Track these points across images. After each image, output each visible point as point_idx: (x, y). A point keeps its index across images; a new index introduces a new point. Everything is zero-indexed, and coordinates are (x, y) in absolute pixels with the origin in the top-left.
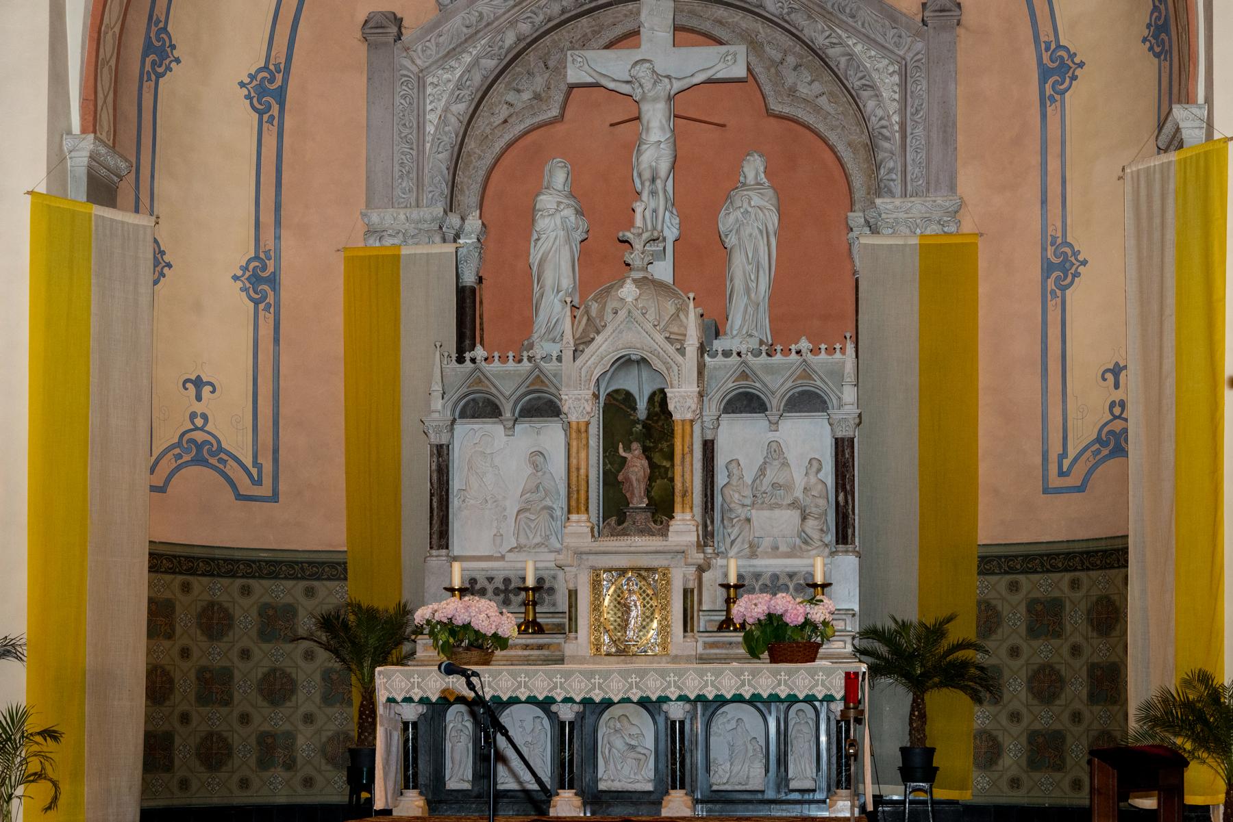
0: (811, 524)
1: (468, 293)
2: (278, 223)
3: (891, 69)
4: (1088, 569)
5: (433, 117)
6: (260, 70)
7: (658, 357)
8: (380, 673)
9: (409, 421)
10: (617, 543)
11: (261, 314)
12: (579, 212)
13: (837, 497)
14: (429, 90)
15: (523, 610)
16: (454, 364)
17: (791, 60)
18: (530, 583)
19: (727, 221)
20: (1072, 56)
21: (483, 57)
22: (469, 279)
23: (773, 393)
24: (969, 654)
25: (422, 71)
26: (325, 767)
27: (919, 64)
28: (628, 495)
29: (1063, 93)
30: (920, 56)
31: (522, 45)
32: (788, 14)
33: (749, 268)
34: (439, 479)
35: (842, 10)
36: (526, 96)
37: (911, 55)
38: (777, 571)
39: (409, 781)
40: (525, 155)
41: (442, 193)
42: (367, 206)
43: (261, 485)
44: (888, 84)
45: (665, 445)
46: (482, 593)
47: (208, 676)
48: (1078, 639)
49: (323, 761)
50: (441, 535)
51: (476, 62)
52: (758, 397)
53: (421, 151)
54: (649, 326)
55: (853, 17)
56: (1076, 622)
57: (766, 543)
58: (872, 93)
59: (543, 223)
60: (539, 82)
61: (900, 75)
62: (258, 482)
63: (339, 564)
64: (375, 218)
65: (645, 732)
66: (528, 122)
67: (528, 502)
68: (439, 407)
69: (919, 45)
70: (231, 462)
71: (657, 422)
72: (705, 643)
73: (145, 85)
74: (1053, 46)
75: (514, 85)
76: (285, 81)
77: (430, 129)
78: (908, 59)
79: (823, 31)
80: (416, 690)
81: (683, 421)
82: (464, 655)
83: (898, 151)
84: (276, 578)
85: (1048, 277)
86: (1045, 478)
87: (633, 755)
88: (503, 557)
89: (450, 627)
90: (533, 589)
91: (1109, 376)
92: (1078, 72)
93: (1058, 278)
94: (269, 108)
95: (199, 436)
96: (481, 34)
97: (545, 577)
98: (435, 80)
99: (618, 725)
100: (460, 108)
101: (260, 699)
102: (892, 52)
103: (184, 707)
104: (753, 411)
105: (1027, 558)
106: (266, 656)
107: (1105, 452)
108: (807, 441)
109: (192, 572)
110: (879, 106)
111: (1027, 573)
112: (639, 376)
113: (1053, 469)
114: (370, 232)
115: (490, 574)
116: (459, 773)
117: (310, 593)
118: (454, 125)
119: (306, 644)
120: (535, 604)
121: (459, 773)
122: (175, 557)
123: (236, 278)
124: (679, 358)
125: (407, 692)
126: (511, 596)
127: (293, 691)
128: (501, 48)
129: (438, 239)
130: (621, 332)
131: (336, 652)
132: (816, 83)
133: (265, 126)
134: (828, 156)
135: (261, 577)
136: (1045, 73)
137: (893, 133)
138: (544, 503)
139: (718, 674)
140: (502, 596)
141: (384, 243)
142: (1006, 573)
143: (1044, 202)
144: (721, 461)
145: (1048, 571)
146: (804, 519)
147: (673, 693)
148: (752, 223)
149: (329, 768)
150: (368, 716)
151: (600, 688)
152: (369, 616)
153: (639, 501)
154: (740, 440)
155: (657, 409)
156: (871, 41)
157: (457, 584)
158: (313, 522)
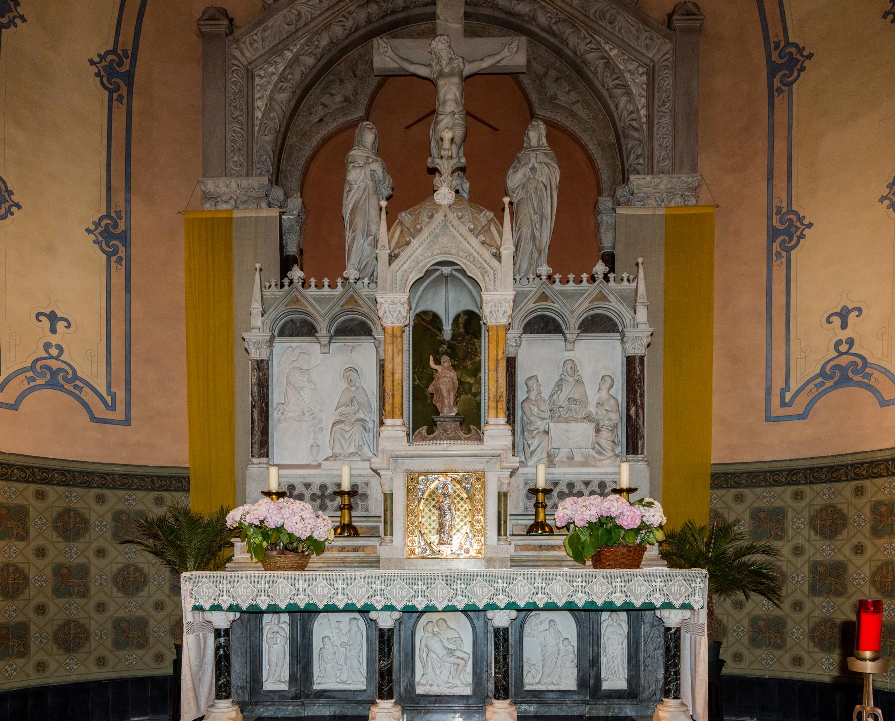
2: (128, 189)
3: (641, 70)
4: (812, 483)
6: (108, 53)
8: (186, 578)
10: (434, 447)
11: (114, 265)
13: (628, 410)
15: (339, 514)
17: (553, 73)
18: (346, 487)
20: (800, 50)
21: (303, 55)
23: (572, 312)
24: (758, 558)
25: (250, 63)
28: (438, 405)
29: (790, 84)
30: (668, 56)
31: (334, 51)
32: (556, 23)
35: (602, 18)
36: (338, 99)
38: (573, 478)
40: (340, 143)
41: (268, 171)
42: (204, 176)
44: (637, 83)
45: (469, 363)
46: (301, 497)
50: (262, 445)
51: (296, 59)
52: (554, 320)
55: (611, 22)
56: (798, 527)
57: (563, 454)
58: (624, 91)
60: (349, 87)
61: (648, 74)
62: (113, 408)
63: (184, 478)
65: (461, 632)
66: (340, 121)
67: (342, 414)
68: (259, 324)
69: (668, 46)
70: (86, 389)
71: (462, 341)
72: (516, 546)
74: (782, 44)
75: (328, 90)
76: (133, 65)
77: (258, 114)
78: (656, 60)
79: (585, 38)
80: (225, 597)
81: (497, 327)
82: (277, 560)
84: (128, 489)
85: (773, 241)
87: (453, 660)
89: (261, 527)
90: (348, 493)
91: (837, 321)
92: (807, 63)
93: (783, 241)
94: (118, 88)
95: (54, 364)
96: (300, 33)
97: (359, 483)
98: (262, 73)
99: (436, 629)
100: (284, 97)
101: (115, 590)
102: (643, 54)
103: (40, 599)
104: (550, 332)
108: (600, 361)
110: (630, 102)
111: (872, 477)
112: (447, 298)
113: (776, 400)
114: (207, 197)
116: (276, 676)
120: (350, 508)
121: (276, 676)
124: (495, 263)
126: (327, 501)
130: (436, 236)
132: (573, 93)
133: (115, 103)
135: (114, 488)
137: (641, 124)
138: (358, 416)
139: (548, 580)
140: (319, 501)
141: (219, 207)
142: (732, 487)
143: (770, 178)
144: (520, 379)
145: (771, 485)
146: (598, 431)
148: (535, 176)
151: (423, 595)
153: (449, 409)
154: (539, 357)
155: (462, 330)
156: (624, 47)
157: (274, 487)
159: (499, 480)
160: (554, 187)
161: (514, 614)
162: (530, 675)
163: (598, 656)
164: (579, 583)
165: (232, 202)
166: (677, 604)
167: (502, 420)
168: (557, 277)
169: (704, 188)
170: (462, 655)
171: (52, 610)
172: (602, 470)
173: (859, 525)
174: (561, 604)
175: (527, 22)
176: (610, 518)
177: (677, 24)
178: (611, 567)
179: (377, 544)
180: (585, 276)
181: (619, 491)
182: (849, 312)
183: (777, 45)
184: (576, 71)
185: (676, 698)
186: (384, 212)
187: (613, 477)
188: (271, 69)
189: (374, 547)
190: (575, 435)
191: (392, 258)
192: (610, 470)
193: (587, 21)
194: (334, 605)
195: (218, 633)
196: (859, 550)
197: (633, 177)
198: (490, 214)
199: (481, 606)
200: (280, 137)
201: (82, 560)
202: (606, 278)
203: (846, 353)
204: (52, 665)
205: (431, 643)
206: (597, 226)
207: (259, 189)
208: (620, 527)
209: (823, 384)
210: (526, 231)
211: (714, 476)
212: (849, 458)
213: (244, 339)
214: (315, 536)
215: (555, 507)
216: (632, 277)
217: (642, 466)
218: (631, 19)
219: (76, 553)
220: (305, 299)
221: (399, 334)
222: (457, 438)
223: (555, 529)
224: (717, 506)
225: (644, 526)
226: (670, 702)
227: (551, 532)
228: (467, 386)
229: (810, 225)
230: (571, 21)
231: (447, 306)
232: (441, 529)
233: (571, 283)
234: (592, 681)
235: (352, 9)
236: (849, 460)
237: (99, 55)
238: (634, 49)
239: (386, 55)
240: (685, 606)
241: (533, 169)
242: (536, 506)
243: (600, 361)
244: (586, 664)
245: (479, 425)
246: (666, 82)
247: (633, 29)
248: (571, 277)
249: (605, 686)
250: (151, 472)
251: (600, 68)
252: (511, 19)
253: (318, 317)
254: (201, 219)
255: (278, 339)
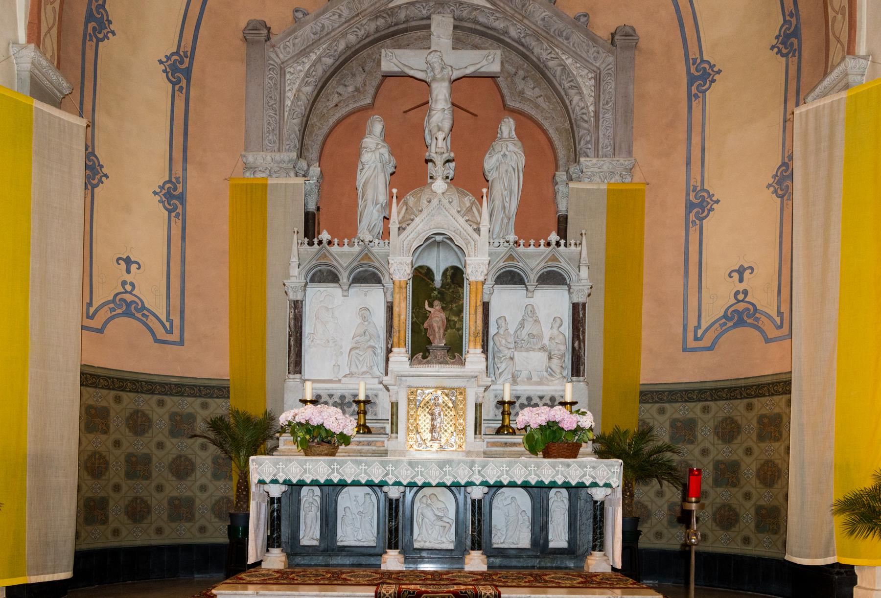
0: (555, 362)
1: (310, 217)
2: (185, 159)
3: (590, 76)
4: (716, 400)
5: (290, 95)
6: (173, 54)
7: (460, 235)
8: (253, 460)
9: (273, 293)
11: (173, 219)
12: (391, 153)
13: (573, 344)
14: (288, 76)
16: (306, 246)
17: (521, 73)
19: (490, 163)
20: (712, 67)
22: (312, 207)
23: (532, 270)
24: (668, 455)
25: (283, 63)
26: (214, 520)
27: (610, 71)
28: (431, 338)
29: (704, 92)
30: (610, 66)
31: (349, 53)
32: (524, 37)
33: (505, 193)
34: (295, 325)
36: (350, 89)
37: (604, 66)
38: (531, 394)
39: (272, 542)
40: (352, 127)
41: (295, 146)
43: (172, 333)
44: (587, 85)
47: (134, 459)
48: (707, 444)
49: (213, 516)
50: (296, 364)
51: (319, 59)
52: (519, 274)
53: (282, 117)
54: (454, 212)
55: (567, 39)
56: (706, 434)
57: (524, 375)
59: (366, 157)
60: (359, 80)
61: (595, 79)
62: (170, 332)
63: (224, 388)
64: (250, 159)
65: (447, 503)
66: (352, 106)
68: (296, 274)
69: (611, 59)
70: (151, 317)
72: (488, 443)
73: (88, 43)
74: (698, 61)
77: (288, 103)
79: (547, 49)
82: (317, 449)
83: (592, 129)
84: (182, 395)
85: (690, 212)
86: (685, 341)
87: (441, 523)
88: (339, 381)
91: (736, 276)
92: (716, 77)
93: (697, 212)
94: (179, 81)
95: (128, 298)
96: (323, 40)
98: (292, 70)
99: (429, 501)
100: (308, 89)
101: (170, 475)
103: (116, 480)
104: (515, 283)
105: (672, 393)
106: (174, 447)
107: (730, 324)
108: (553, 304)
109: (123, 389)
113: (690, 335)
114: (247, 167)
115: (331, 392)
116: (310, 533)
117: (205, 406)
118: (303, 102)
119: (201, 440)
122: (110, 378)
123: (155, 193)
124: (476, 236)
125: (274, 475)
127: (193, 470)
128: (336, 51)
129: (292, 174)
130: (433, 216)
131: (220, 446)
133: (177, 93)
134: (541, 137)
135: (171, 395)
136: (691, 80)
137: (589, 117)
138: (369, 343)
139: (510, 465)
142: (656, 402)
143: (688, 163)
145: (686, 401)
146: (550, 358)
147: (477, 480)
148: (506, 160)
149: (217, 520)
150: (243, 490)
151: (422, 475)
152: (246, 421)
153: (439, 341)
154: (507, 303)
155: (449, 280)
156: (577, 57)
158: (206, 358)
159: (476, 394)
160: (520, 170)
161: (486, 489)
162: (496, 537)
163: (547, 523)
164: (533, 468)
165: (267, 171)
166: (601, 484)
167: (479, 350)
168: (522, 242)
169: (637, 168)
170: (447, 520)
171: (124, 489)
172: (553, 388)
173: (749, 432)
174: (519, 483)
175: (502, 34)
176: (555, 423)
177: (618, 43)
178: (556, 457)
179: (386, 440)
180: (542, 242)
181: (561, 404)
182: (745, 269)
183: (695, 61)
184: (540, 71)
185: (600, 551)
186: (395, 197)
187: (561, 393)
188: (299, 68)
189: (383, 442)
190: (535, 361)
191: (401, 229)
192: (559, 388)
193: (548, 36)
194: (358, 481)
195: (272, 500)
196: (749, 451)
197: (582, 159)
198: (472, 198)
199: (463, 483)
200: (305, 119)
201: (146, 451)
202: (558, 244)
203: (743, 301)
204: (124, 532)
205: (425, 511)
206: (555, 193)
207: (289, 162)
208: (563, 429)
209: (725, 324)
210: (498, 203)
211: (642, 394)
212: (743, 381)
213: (284, 285)
214: (345, 432)
215: (517, 414)
216: (578, 242)
217: (582, 385)
218: (582, 37)
219: (142, 445)
220: (331, 255)
221: (404, 286)
222: (446, 363)
223: (517, 431)
224: (645, 417)
225: (579, 429)
226: (597, 554)
227: (514, 433)
228: (452, 323)
229: (718, 202)
230: (536, 36)
231: (438, 263)
232: (433, 429)
233: (532, 246)
234: (542, 542)
235: (364, 22)
236: (742, 383)
237: (166, 56)
238: (586, 60)
239: (393, 60)
240: (607, 485)
241: (504, 155)
242: (503, 413)
243: (553, 304)
244: (537, 529)
245: (461, 352)
246: (610, 86)
247: (584, 44)
248: (532, 242)
249: (552, 545)
250: (198, 383)
251: (558, 73)
252: (490, 32)
253: (341, 269)
254: (242, 185)
255: (309, 285)
